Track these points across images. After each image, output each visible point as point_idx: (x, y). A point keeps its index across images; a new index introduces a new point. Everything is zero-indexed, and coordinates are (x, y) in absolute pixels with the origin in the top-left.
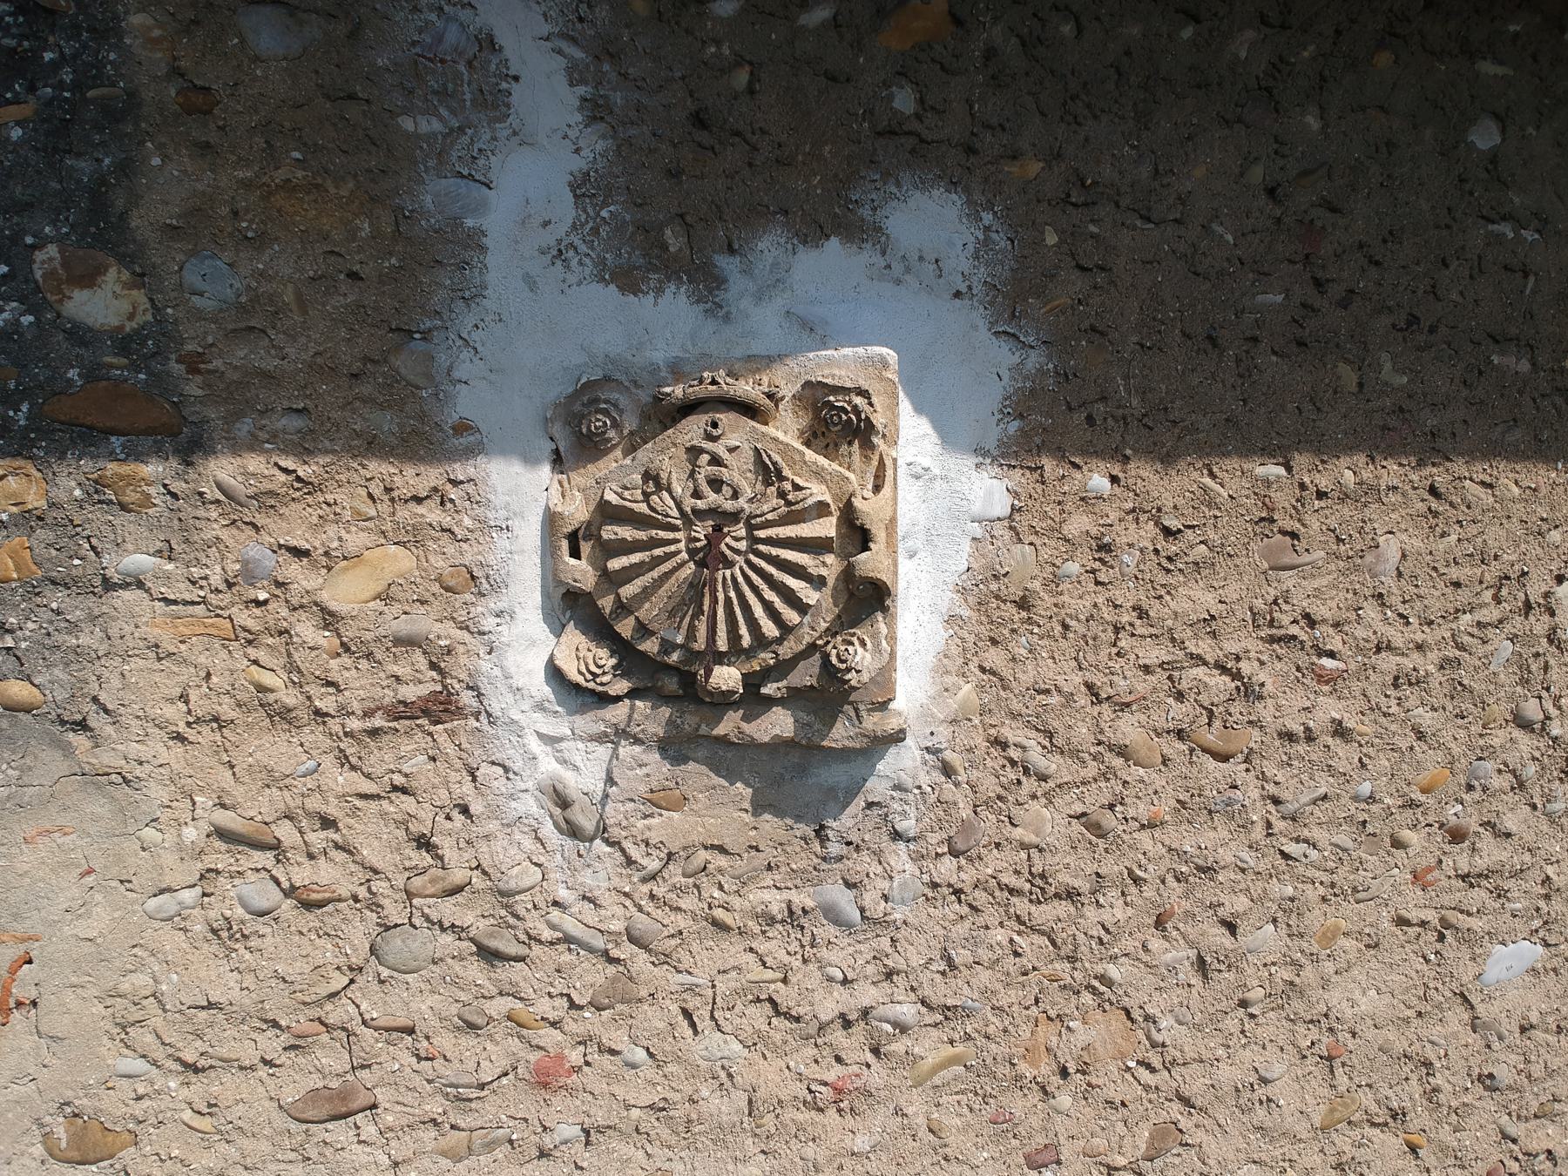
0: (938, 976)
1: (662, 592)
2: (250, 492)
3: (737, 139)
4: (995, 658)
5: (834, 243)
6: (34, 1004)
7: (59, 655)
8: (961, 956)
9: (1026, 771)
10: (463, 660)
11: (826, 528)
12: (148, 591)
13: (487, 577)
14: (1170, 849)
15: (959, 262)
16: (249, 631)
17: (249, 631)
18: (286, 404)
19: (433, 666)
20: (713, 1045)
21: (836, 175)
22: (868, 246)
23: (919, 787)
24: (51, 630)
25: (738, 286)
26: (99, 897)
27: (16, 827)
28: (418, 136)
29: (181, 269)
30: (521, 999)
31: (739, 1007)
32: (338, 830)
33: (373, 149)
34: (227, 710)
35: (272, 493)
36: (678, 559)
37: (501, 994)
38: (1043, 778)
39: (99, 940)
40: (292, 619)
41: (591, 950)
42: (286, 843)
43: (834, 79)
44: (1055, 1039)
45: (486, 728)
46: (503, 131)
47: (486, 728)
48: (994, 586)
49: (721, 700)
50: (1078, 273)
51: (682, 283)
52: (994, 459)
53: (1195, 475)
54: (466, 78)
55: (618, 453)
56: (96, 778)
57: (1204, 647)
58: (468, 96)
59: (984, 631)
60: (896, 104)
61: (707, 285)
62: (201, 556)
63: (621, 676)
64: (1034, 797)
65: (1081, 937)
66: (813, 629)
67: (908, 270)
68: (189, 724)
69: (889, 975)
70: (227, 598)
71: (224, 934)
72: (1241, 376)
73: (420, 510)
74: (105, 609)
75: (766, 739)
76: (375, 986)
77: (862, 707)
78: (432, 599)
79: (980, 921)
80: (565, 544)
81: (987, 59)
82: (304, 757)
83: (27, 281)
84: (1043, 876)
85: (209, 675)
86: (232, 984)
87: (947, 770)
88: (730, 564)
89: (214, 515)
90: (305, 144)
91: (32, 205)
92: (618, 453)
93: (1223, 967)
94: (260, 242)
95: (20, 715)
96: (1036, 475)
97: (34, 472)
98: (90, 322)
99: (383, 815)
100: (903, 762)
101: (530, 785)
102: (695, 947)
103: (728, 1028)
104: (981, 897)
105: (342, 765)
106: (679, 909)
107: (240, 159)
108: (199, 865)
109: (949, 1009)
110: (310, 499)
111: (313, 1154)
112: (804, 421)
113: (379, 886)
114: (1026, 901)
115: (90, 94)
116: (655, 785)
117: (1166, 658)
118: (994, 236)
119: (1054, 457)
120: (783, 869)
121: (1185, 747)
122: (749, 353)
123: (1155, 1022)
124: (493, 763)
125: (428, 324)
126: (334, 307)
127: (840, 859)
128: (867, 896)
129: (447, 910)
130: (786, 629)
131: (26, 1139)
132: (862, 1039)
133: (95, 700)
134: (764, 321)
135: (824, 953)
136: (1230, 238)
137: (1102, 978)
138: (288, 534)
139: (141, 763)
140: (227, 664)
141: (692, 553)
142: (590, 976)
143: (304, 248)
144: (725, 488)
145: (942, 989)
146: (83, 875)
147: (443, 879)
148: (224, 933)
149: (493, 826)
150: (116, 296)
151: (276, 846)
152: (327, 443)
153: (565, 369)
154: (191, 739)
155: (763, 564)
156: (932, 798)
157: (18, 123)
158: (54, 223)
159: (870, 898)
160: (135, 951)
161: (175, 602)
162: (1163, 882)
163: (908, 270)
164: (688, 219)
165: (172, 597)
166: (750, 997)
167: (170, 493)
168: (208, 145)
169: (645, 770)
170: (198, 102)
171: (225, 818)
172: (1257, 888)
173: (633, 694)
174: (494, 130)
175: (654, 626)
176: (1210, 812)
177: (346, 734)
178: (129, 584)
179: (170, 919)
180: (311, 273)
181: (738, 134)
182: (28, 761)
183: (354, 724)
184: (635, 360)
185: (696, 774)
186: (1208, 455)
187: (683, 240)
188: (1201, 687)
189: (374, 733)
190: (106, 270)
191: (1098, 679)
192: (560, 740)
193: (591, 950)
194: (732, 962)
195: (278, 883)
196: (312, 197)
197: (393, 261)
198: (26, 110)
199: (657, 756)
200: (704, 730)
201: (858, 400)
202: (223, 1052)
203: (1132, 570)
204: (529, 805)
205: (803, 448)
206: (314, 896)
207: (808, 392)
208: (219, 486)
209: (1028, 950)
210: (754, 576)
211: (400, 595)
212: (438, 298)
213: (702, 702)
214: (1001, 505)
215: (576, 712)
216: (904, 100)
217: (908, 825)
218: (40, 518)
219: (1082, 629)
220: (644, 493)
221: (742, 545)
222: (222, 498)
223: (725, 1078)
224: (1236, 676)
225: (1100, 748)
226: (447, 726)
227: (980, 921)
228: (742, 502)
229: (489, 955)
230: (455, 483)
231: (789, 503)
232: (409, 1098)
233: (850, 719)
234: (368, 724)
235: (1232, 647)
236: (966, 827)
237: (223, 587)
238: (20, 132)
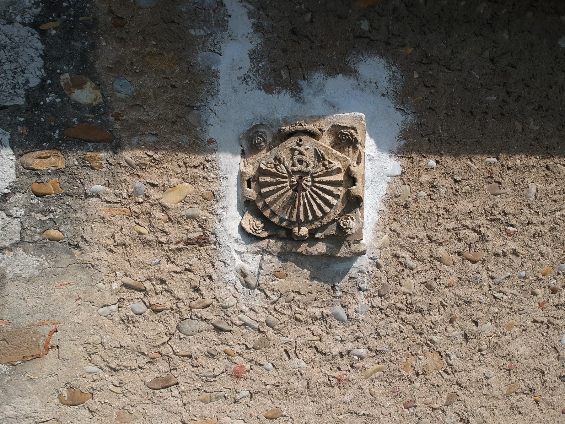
4: (395, 226)
8: (382, 332)
9: (406, 266)
10: (210, 224)
11: (340, 177)
19: (200, 226)
20: (296, 363)
23: (368, 272)
25: (307, 91)
26: (82, 308)
34: (128, 241)
36: (286, 188)
38: (411, 269)
41: (253, 328)
45: (218, 248)
46: (225, 35)
47: (218, 248)
48: (395, 200)
49: (301, 239)
50: (425, 88)
52: (396, 154)
55: (265, 151)
59: (391, 216)
61: (296, 91)
63: (265, 230)
64: (408, 276)
66: (334, 214)
67: (366, 86)
73: (196, 171)
75: (316, 253)
77: (351, 242)
79: (389, 320)
80: (246, 183)
84: (411, 304)
87: (378, 266)
88: (305, 190)
92: (265, 151)
96: (410, 160)
99: (182, 279)
100: (363, 262)
101: (233, 269)
102: (289, 328)
104: (389, 312)
111: (156, 401)
112: (332, 139)
116: (276, 269)
120: (320, 300)
124: (220, 261)
125: (199, 104)
127: (340, 297)
130: (325, 213)
131: (53, 397)
133: (82, 237)
134: (316, 104)
137: (431, 341)
141: (291, 186)
142: (253, 338)
144: (304, 163)
147: (203, 302)
148: (126, 321)
149: (220, 283)
151: (144, 290)
153: (247, 121)
155: (317, 190)
156: (373, 276)
163: (366, 86)
169: (273, 264)
170: (119, 23)
173: (269, 237)
175: (277, 213)
181: (307, 37)
183: (173, 246)
184: (271, 117)
185: (290, 266)
189: (180, 250)
191: (431, 234)
192: (243, 253)
197: (187, 81)
198: (57, 24)
199: (277, 259)
200: (294, 250)
201: (352, 131)
202: (125, 364)
204: (232, 276)
205: (332, 149)
208: (126, 161)
210: (314, 195)
211: (189, 201)
213: (293, 240)
214: (398, 171)
216: (365, 25)
217: (364, 285)
219: (426, 216)
221: (310, 184)
223: (300, 375)
225: (432, 259)
227: (389, 320)
228: (310, 168)
229: (218, 330)
230: (208, 161)
231: (327, 168)
232: (189, 381)
233: (346, 246)
234: (178, 247)
236: (384, 286)
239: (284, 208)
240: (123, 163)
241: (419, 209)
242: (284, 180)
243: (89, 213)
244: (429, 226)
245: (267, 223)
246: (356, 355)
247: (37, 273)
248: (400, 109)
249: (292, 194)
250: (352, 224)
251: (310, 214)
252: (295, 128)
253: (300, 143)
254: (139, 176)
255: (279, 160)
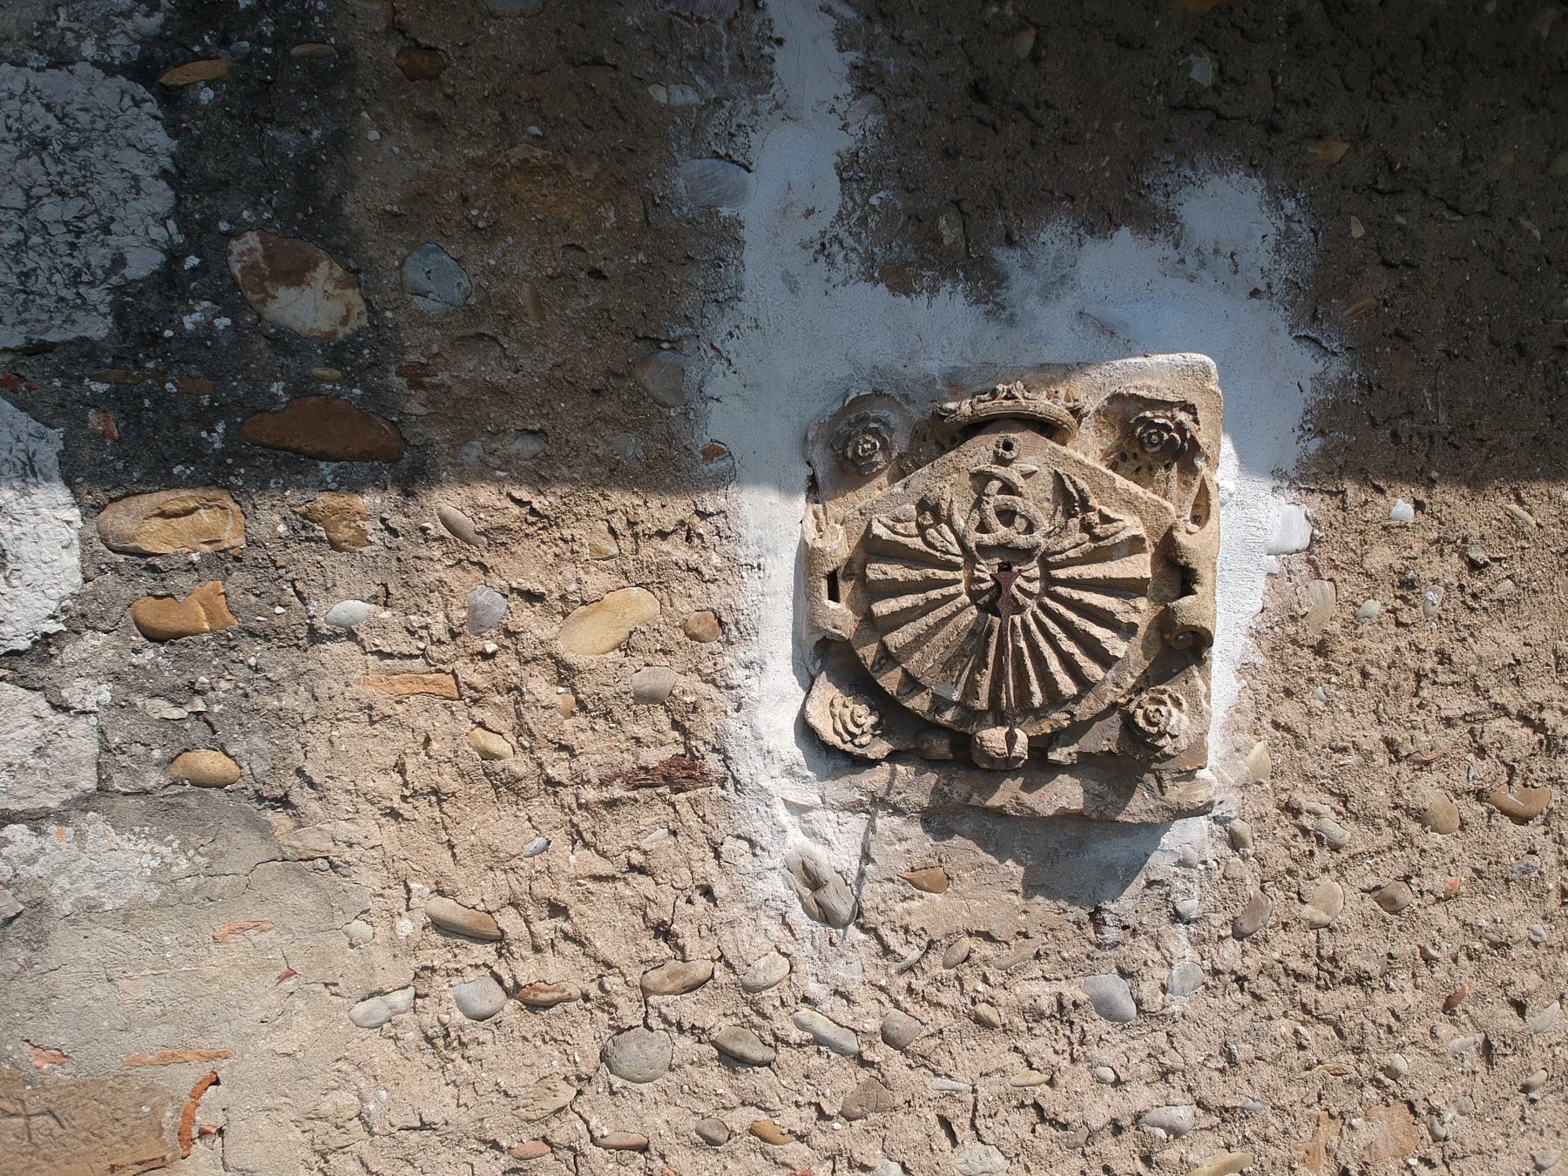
0: (1217, 1074)
1: (936, 640)
2: (480, 527)
3: (1020, 115)
4: (1289, 712)
5: (1124, 233)
6: (221, 1132)
7: (257, 720)
8: (1243, 1051)
9: (1319, 839)
10: (709, 718)
11: (1139, 567)
12: (360, 643)
13: (737, 623)
14: (1465, 924)
15: (1258, 255)
16: (476, 689)
17: (476, 689)
18: (520, 425)
19: (676, 725)
21: (1127, 156)
22: (1159, 237)
23: (1204, 862)
24: (249, 690)
25: (1021, 284)
26: (300, 1004)
27: (205, 926)
28: (670, 109)
29: (402, 265)
30: (766, 1110)
31: (1002, 1114)
32: (568, 917)
33: (620, 123)
34: (448, 782)
35: (504, 529)
36: (958, 602)
37: (743, 1104)
38: (1336, 848)
39: (299, 1055)
40: (524, 674)
41: (843, 1052)
42: (511, 934)
43: (1127, 45)
44: (1335, 1138)
45: (733, 796)
47: (733, 796)
48: (1291, 629)
51: (959, 280)
52: (1292, 482)
53: (1502, 500)
54: (725, 40)
55: (883, 479)
56: (299, 863)
57: (1506, 695)
58: (726, 63)
59: (1279, 683)
60: (1194, 75)
62: (422, 602)
63: (880, 736)
64: (1325, 870)
65: (1369, 1026)
66: (1118, 685)
67: (1202, 265)
68: (404, 798)
69: (1165, 1074)
70: (450, 650)
71: (440, 1042)
72: (1548, 389)
73: (665, 546)
74: (310, 665)
75: (1050, 812)
76: (606, 1098)
77: (1166, 776)
78: (676, 648)
79: (1263, 1011)
80: (824, 584)
81: (1290, 25)
82: (532, 833)
83: (222, 276)
84: (1333, 959)
85: (428, 740)
86: (447, 1100)
87: (1235, 842)
88: (1020, 609)
89: (437, 554)
90: (545, 118)
91: (227, 184)
92: (883, 479)
93: (1509, 1051)
94: (490, 234)
95: (212, 791)
96: (1337, 501)
97: (231, 504)
98: (297, 326)
99: (618, 899)
100: (1190, 836)
101: (778, 862)
103: (989, 1138)
104: (1265, 985)
105: (574, 842)
106: (939, 1005)
107: (471, 134)
108: (414, 963)
109: (1227, 1110)
110: (544, 535)
112: (1109, 441)
113: (613, 982)
114: (1312, 987)
115: (295, 51)
116: (916, 863)
117: (1469, 709)
118: (1295, 226)
119: (1356, 480)
120: (1053, 958)
121: (1483, 809)
122: (1040, 361)
123: (1439, 1115)
124: (739, 837)
125: (679, 332)
126: (575, 312)
127: (1115, 945)
128: (1144, 987)
129: (687, 1008)
132: (1132, 1146)
133: (300, 772)
134: (1054, 326)
135: (1094, 1052)
136: (1537, 233)
138: (521, 575)
139: (351, 845)
140: (449, 727)
141: (974, 596)
142: (842, 1081)
143: (541, 241)
144: (1018, 520)
145: (1221, 1088)
146: (281, 979)
147: (684, 973)
148: (440, 1041)
149: (737, 910)
150: (328, 297)
151: (499, 940)
152: (565, 470)
153: (827, 383)
154: (407, 815)
155: (1062, 610)
156: (1218, 875)
157: (209, 83)
158: (254, 206)
159: (1148, 990)
160: (339, 1065)
161: (390, 656)
162: (1455, 960)
163: (1202, 265)
164: (965, 206)
165: (388, 650)
166: (1014, 1102)
167: (389, 529)
168: (434, 117)
169: (905, 845)
170: (422, 65)
171: (445, 908)
172: (1547, 964)
173: (893, 757)
174: (755, 102)
176: (1507, 881)
177: (580, 806)
178: (338, 636)
179: (380, 1026)
180: (550, 271)
181: (1020, 108)
182: (219, 845)
183: (590, 794)
186: (1516, 478)
187: (958, 230)
188: (1504, 741)
189: (611, 804)
190: (316, 265)
191: (1399, 735)
192: (808, 809)
193: (843, 1052)
194: (995, 1064)
195: (499, 980)
196: (551, 181)
197: (641, 256)
198: (218, 68)
199: (919, 829)
200: (976, 799)
201: (1182, 416)
203: (1437, 609)
204: (776, 886)
205: (1110, 472)
206: (542, 997)
207: (1116, 407)
208: (445, 521)
209: (1312, 1042)
211: (643, 645)
212: (687, 304)
213: (976, 767)
214: (1300, 539)
215: (828, 777)
218: (237, 559)
220: (919, 526)
221: (1035, 587)
222: (447, 534)
224: (1539, 727)
225: (1397, 813)
226: (690, 794)
227: (1263, 1011)
228: (1038, 536)
229: (731, 1060)
230: (704, 515)
231: (1095, 538)
233: (1150, 790)
234: (606, 794)
235: (1535, 695)
236: (1254, 907)
237: (446, 637)
238: (211, 94)
239: (947, 666)
240: (436, 528)
241: (1363, 657)
242: (950, 575)
243: (322, 692)
244: (1391, 710)
245: (890, 714)
246: (1162, 1127)
247: (154, 894)
248: (1307, 337)
249: (977, 620)
250: (1178, 720)
251: (1035, 687)
252: (988, 407)
253: (1008, 455)
254: (485, 569)
255: (935, 510)
